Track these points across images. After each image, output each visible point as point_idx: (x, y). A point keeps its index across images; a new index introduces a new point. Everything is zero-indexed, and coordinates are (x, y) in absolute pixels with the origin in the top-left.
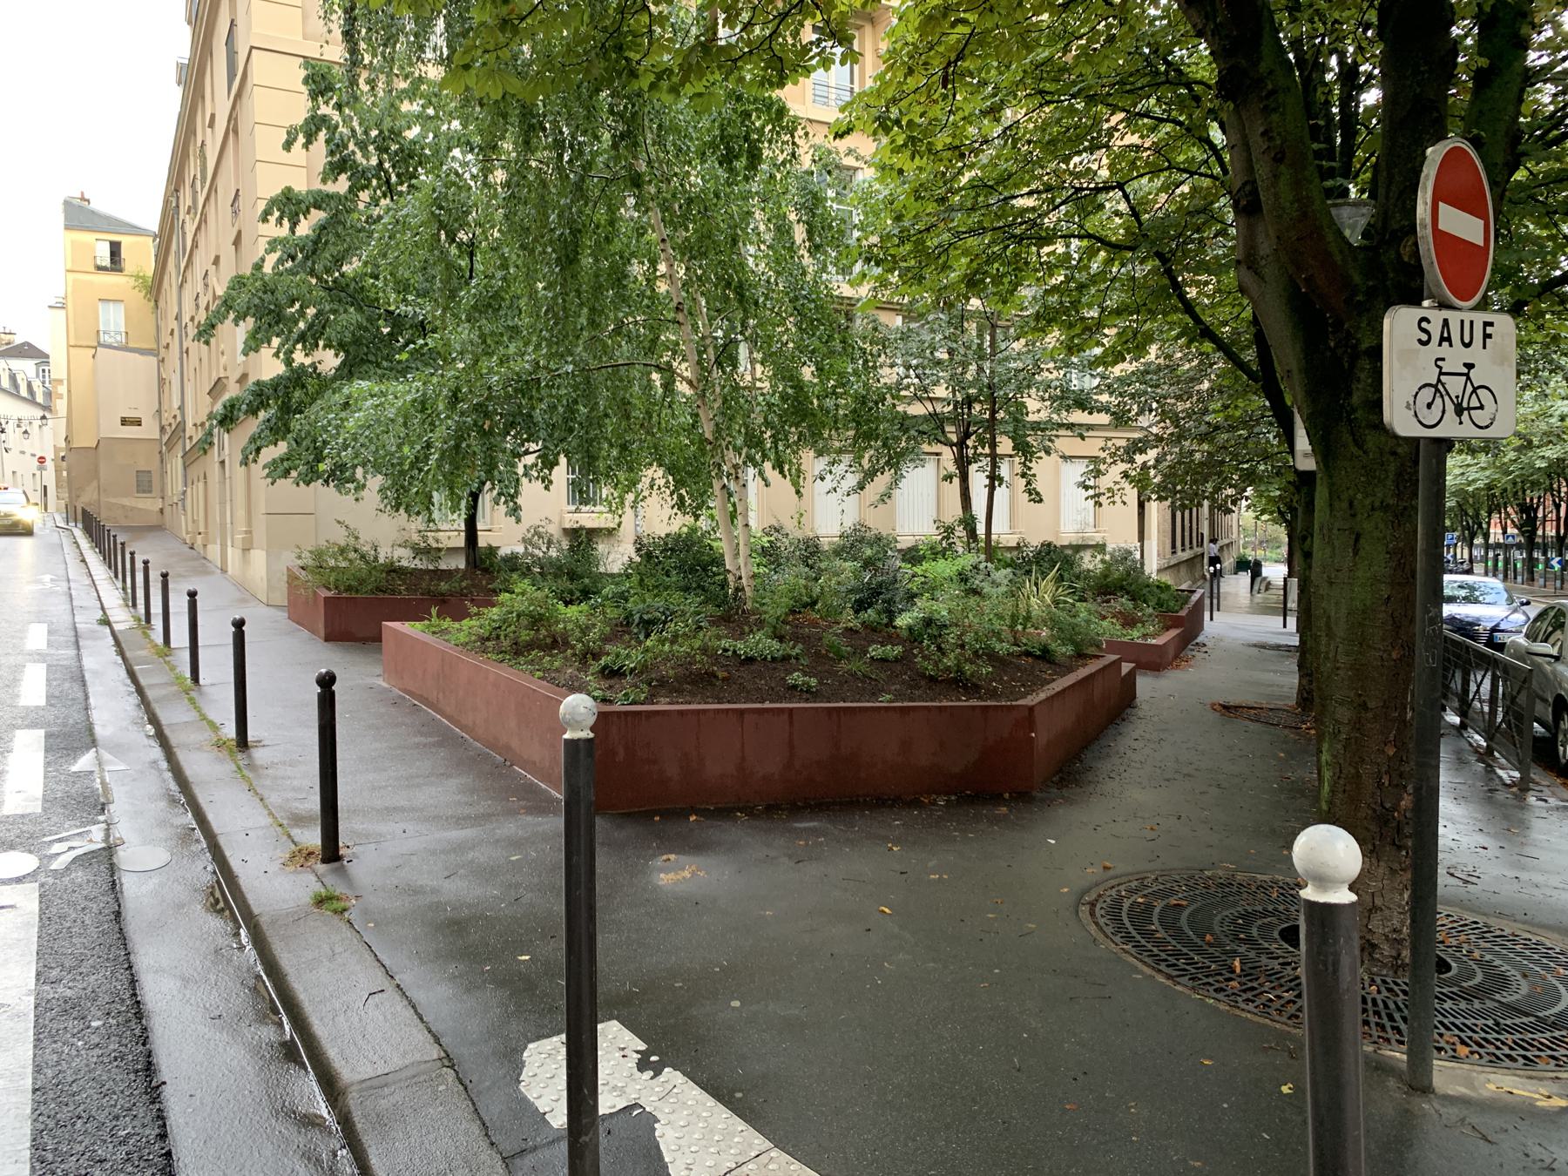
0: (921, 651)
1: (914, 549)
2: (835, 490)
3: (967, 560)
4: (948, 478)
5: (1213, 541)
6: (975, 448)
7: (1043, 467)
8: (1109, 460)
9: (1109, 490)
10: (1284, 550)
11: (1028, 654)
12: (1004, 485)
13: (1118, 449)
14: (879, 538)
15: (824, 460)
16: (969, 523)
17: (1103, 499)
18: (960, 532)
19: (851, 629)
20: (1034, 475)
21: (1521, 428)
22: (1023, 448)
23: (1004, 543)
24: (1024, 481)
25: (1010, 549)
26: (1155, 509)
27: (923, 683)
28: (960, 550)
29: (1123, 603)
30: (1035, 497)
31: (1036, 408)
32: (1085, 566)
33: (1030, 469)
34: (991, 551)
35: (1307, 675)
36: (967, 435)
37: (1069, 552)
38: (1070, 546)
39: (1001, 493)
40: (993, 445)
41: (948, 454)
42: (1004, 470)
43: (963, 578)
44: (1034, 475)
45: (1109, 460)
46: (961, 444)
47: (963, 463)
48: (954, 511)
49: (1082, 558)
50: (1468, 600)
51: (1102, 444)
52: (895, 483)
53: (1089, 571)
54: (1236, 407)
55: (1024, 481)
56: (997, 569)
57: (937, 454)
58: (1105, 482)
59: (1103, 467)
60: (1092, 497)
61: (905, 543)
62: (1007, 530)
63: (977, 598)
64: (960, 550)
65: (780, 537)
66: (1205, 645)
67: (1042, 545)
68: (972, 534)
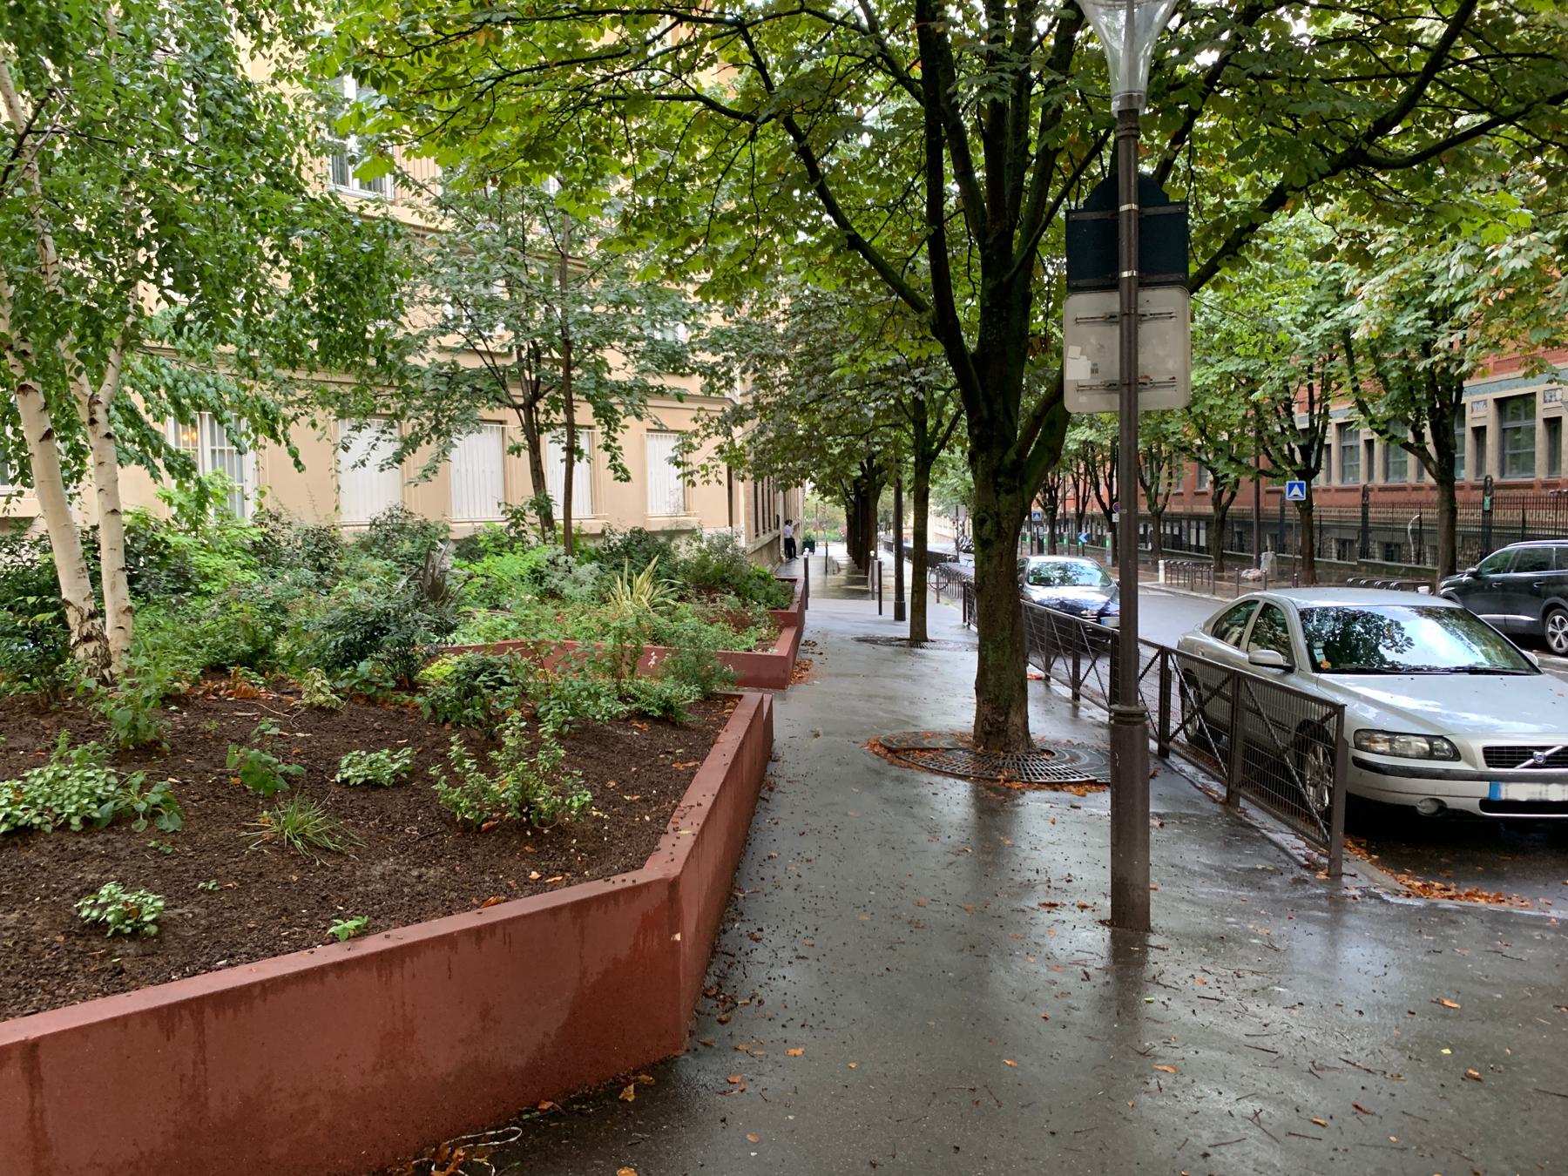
0: (447, 769)
1: (473, 540)
2: (363, 463)
3: (542, 553)
4: (516, 450)
5: (788, 522)
6: (547, 412)
7: (631, 434)
8: (702, 433)
9: (703, 467)
10: (843, 529)
11: (642, 715)
12: (584, 460)
13: (711, 420)
14: (425, 527)
15: (348, 423)
16: (543, 507)
17: (696, 478)
18: (532, 517)
19: (320, 708)
20: (620, 448)
21: (503, 508)
22: (606, 414)
23: (586, 530)
24: (608, 455)
25: (595, 536)
26: (743, 490)
27: (449, 840)
28: (533, 540)
29: (730, 601)
30: (622, 474)
31: (619, 365)
32: (681, 557)
33: (614, 440)
34: (571, 540)
35: (989, 701)
36: (537, 396)
37: (662, 540)
38: (663, 533)
39: (580, 468)
40: (570, 410)
41: (514, 420)
42: (583, 443)
43: (537, 576)
44: (620, 448)
45: (702, 433)
46: (529, 406)
47: (533, 433)
48: (524, 491)
49: (678, 547)
50: (1064, 581)
51: (694, 414)
52: (444, 453)
53: (686, 561)
54: (865, 360)
55: (608, 455)
56: (580, 563)
57: (501, 422)
58: (696, 459)
59: (695, 441)
60: (684, 475)
61: (461, 531)
62: (587, 514)
63: (556, 602)
64: (533, 540)
65: (279, 527)
66: (815, 644)
67: (632, 532)
68: (548, 520)
